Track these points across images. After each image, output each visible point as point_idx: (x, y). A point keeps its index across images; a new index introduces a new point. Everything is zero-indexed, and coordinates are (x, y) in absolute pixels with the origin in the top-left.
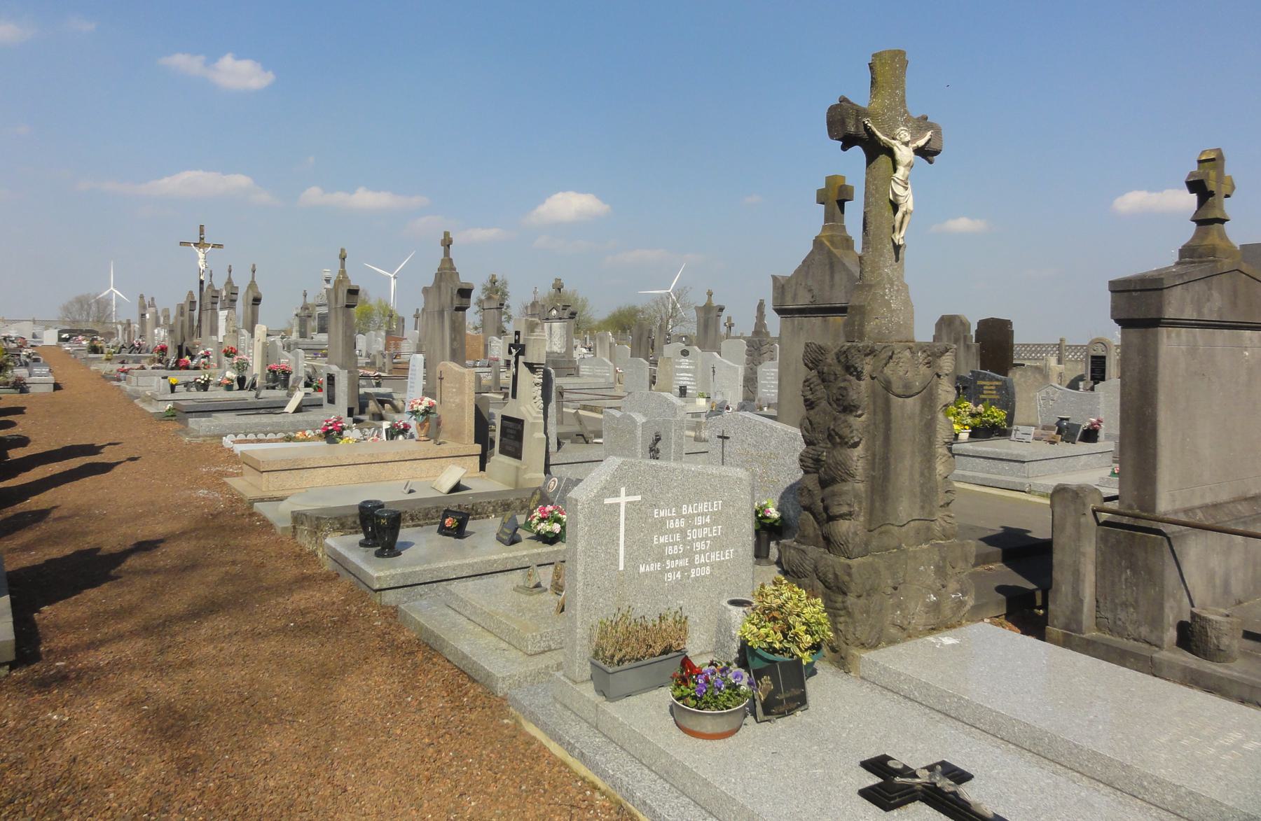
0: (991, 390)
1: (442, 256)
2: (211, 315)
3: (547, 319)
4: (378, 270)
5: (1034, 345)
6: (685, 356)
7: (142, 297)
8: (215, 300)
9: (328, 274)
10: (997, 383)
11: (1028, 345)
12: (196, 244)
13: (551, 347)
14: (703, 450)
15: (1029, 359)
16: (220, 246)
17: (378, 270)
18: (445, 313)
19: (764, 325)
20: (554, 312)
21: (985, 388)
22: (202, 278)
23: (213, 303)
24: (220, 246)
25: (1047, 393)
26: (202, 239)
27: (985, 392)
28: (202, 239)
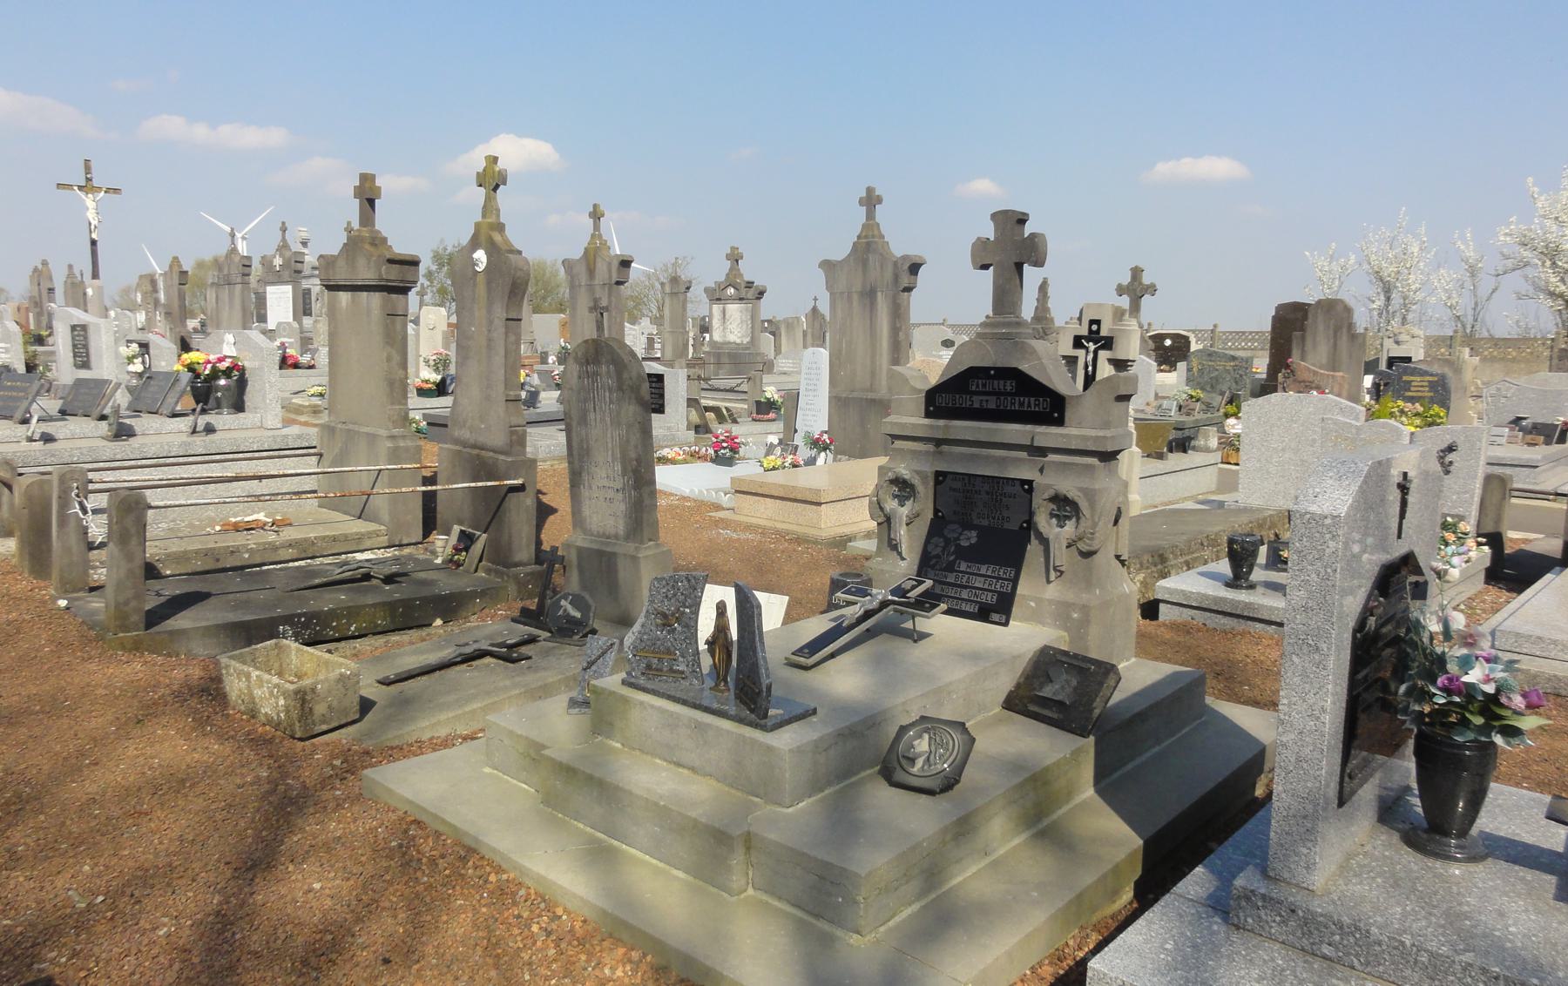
0: (1422, 386)
1: (864, 220)
2: (243, 292)
3: (719, 299)
4: (219, 224)
5: (1251, 333)
6: (947, 347)
7: (70, 267)
8: (246, 270)
9: (304, 235)
10: (1431, 379)
11: (1244, 333)
12: (80, 188)
13: (725, 336)
14: (1212, 462)
15: (1245, 349)
16: (116, 191)
17: (219, 224)
18: (879, 294)
19: (1047, 310)
20: (731, 291)
21: (1413, 384)
22: (94, 236)
23: (244, 275)
24: (116, 191)
25: (1499, 389)
26: (89, 180)
27: (1412, 389)
28: (89, 180)
